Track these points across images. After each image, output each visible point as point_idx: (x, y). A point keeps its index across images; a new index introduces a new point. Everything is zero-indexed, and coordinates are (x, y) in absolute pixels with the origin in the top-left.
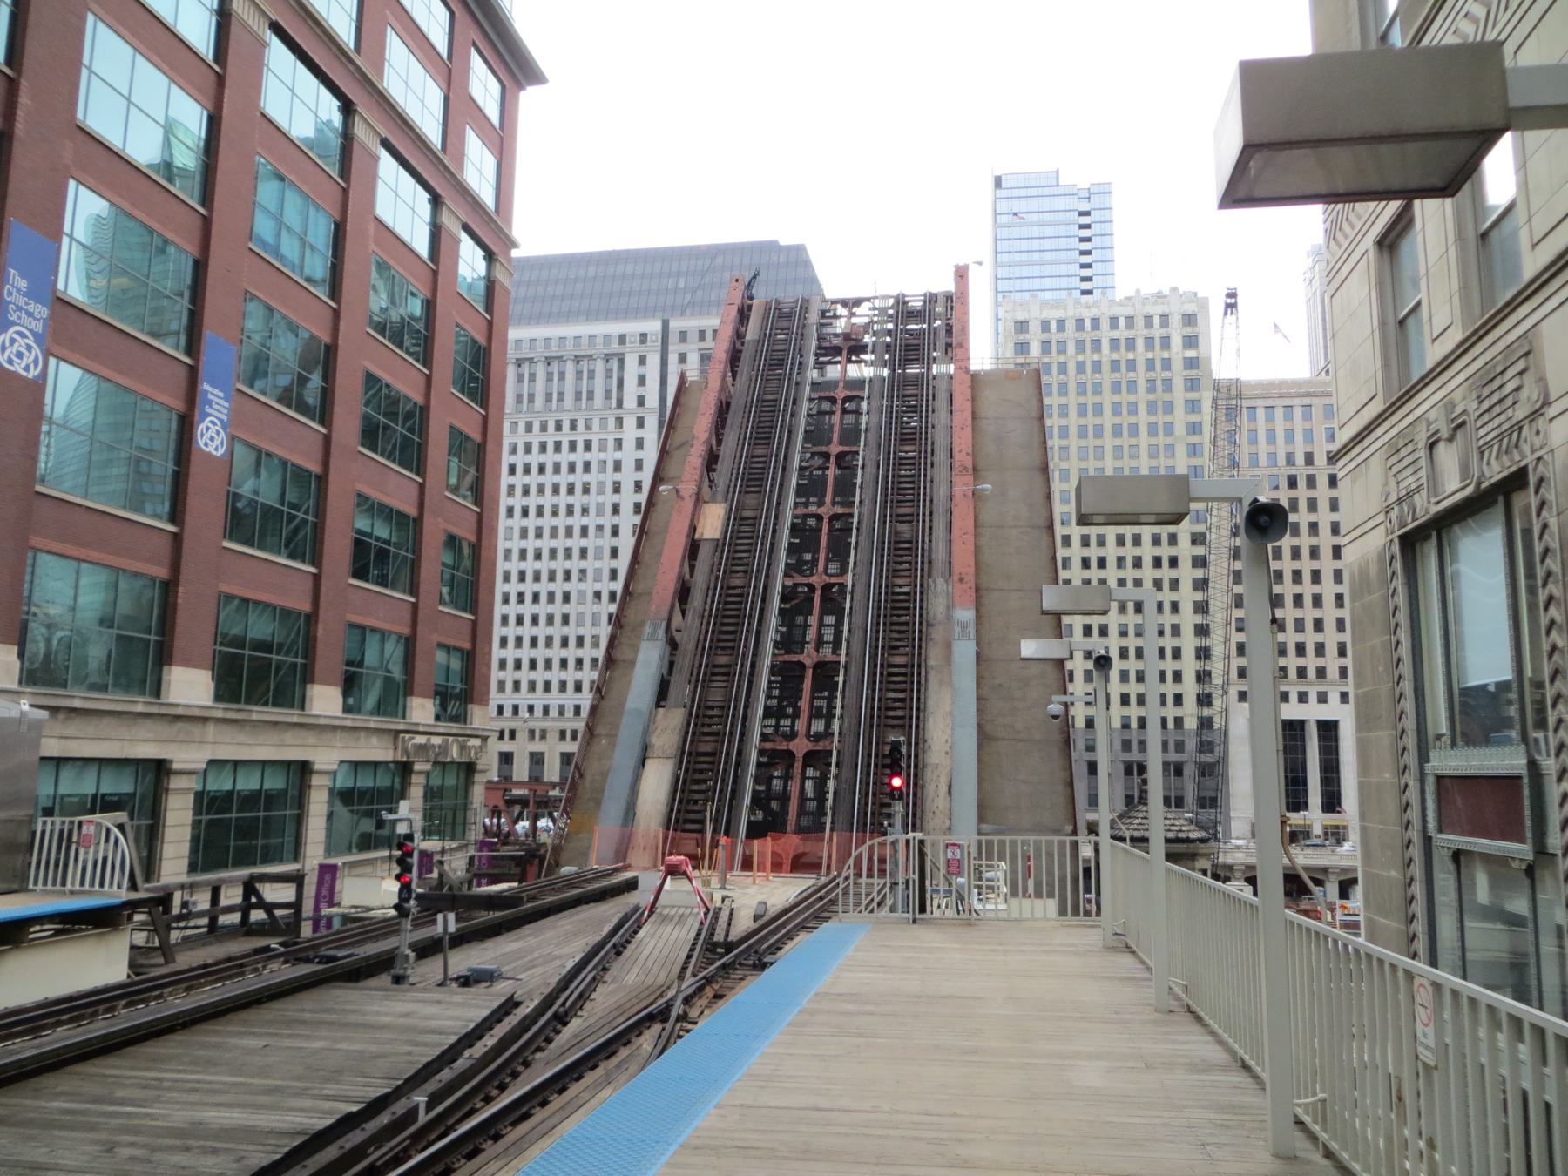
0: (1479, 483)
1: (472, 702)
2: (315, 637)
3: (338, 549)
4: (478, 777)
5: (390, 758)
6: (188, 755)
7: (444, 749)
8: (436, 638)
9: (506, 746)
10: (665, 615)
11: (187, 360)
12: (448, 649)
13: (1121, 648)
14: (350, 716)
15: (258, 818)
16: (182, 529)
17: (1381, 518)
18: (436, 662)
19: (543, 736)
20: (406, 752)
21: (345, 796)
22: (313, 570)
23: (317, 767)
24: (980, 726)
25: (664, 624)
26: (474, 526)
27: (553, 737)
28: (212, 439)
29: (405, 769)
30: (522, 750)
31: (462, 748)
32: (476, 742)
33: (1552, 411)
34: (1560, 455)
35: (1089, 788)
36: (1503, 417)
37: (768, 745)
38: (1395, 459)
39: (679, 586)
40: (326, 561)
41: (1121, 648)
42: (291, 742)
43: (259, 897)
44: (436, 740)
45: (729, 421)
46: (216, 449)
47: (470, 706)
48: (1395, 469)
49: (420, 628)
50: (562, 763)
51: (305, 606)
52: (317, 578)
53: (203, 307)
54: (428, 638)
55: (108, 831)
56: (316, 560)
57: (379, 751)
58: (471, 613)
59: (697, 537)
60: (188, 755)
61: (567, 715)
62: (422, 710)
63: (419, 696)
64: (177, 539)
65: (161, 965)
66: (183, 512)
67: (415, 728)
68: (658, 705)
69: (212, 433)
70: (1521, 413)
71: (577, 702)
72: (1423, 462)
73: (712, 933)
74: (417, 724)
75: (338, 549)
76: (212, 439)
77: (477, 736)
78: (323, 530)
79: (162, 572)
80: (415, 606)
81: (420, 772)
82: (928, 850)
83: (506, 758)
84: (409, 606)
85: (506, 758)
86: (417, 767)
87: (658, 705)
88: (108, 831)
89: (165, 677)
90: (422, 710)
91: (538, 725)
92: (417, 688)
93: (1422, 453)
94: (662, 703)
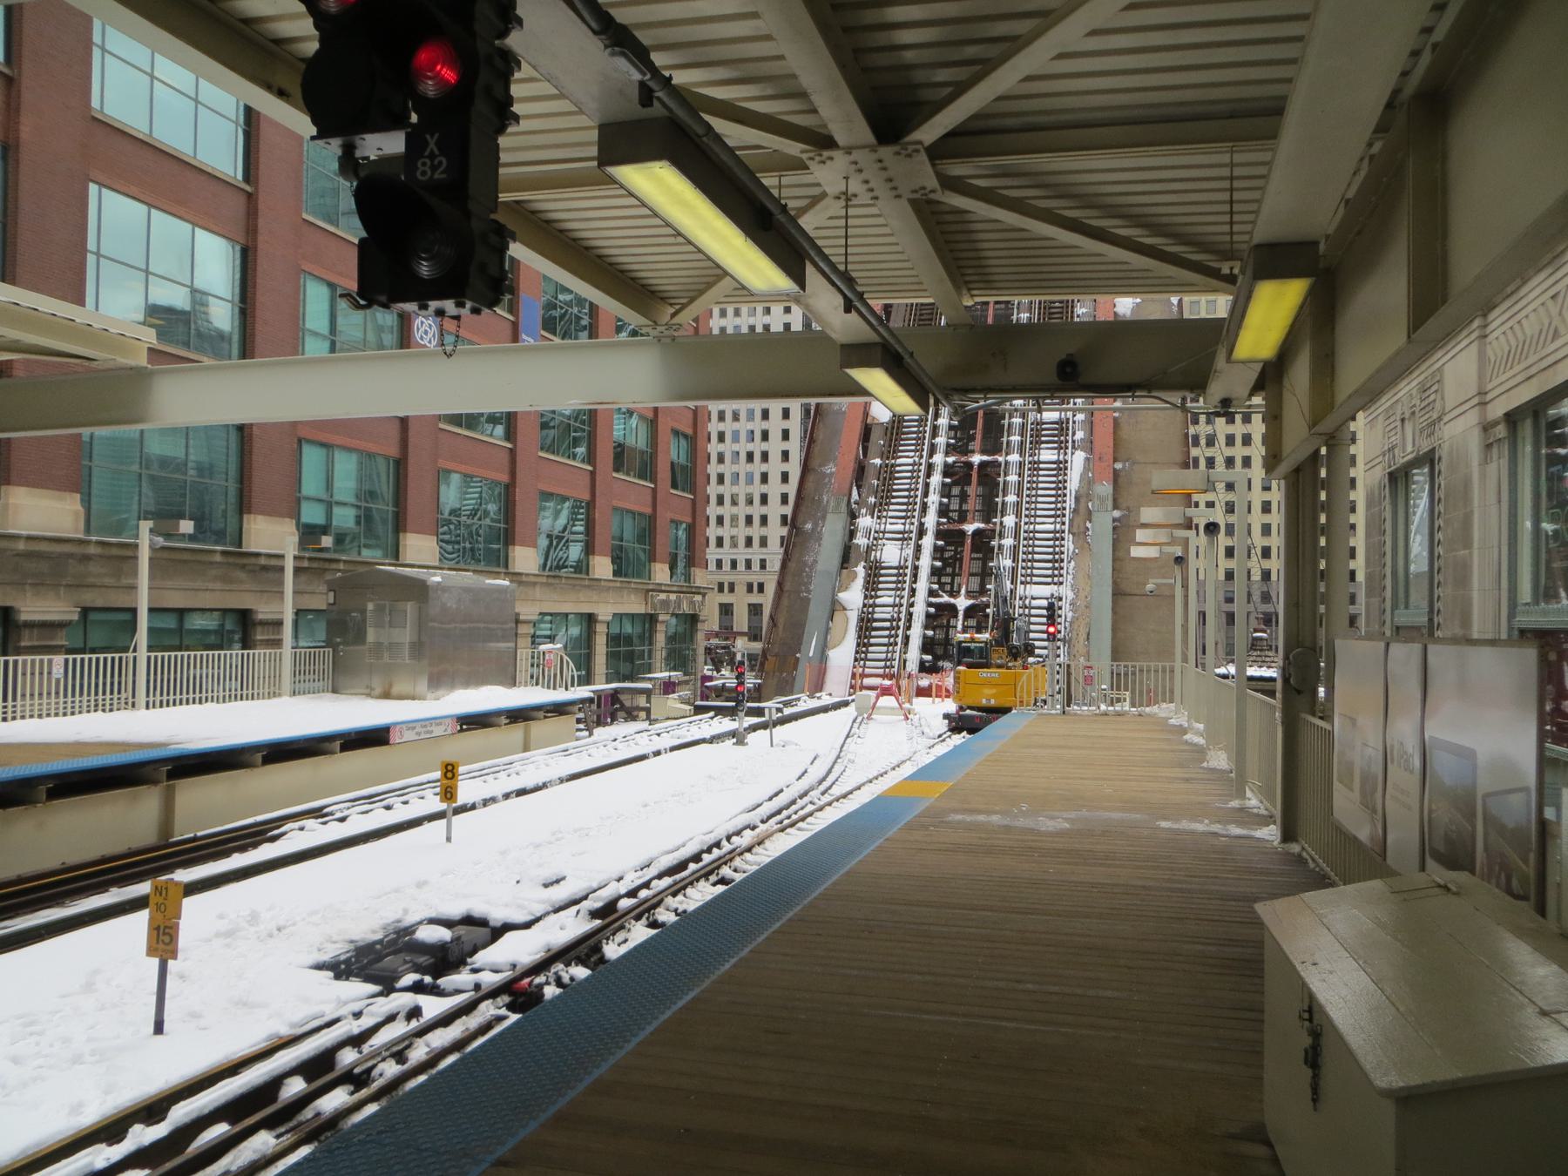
0: (1419, 451)
1: (655, 561)
2: (594, 519)
3: (664, 474)
4: (700, 626)
5: (643, 611)
6: (605, 612)
7: (678, 603)
8: (670, 515)
9: (726, 598)
10: (847, 492)
11: (511, 318)
12: (623, 512)
13: (1264, 502)
14: (620, 579)
15: (620, 652)
16: (515, 445)
17: (1381, 459)
18: (670, 536)
19: (732, 589)
20: (654, 607)
21: (639, 637)
22: (590, 468)
23: (600, 618)
24: (1115, 583)
25: (846, 498)
26: (690, 421)
27: (741, 589)
28: (426, 333)
29: (651, 619)
30: (741, 602)
31: (692, 603)
32: (698, 598)
33: (1446, 419)
34: (1446, 446)
35: (1227, 638)
36: (1427, 416)
37: (933, 600)
38: (1388, 422)
39: (857, 466)
40: (520, 437)
41: (1264, 502)
42: (582, 599)
43: (622, 705)
44: (673, 597)
45: (893, 314)
46: (430, 342)
47: (692, 569)
48: (1388, 429)
49: (659, 508)
50: (721, 614)
51: (648, 510)
52: (593, 474)
53: (519, 275)
54: (664, 516)
55: (561, 657)
56: (653, 480)
57: (636, 606)
58: (651, 481)
59: (868, 421)
60: (605, 612)
61: (738, 569)
62: (661, 573)
63: (263, 513)
64: (512, 452)
65: (586, 738)
66: (515, 433)
67: (658, 588)
68: (842, 567)
69: (425, 327)
70: (1435, 416)
71: (734, 557)
72: (1399, 428)
73: (727, 859)
74: (661, 584)
75: (664, 474)
76: (426, 333)
77: (699, 593)
78: (595, 436)
79: (504, 478)
80: (654, 491)
81: (663, 622)
82: (1073, 671)
83: (726, 610)
84: (650, 490)
85: (726, 610)
86: (661, 618)
87: (842, 567)
88: (561, 657)
89: (510, 554)
90: (661, 573)
91: (726, 579)
92: (658, 556)
93: (1399, 423)
94: (845, 565)
